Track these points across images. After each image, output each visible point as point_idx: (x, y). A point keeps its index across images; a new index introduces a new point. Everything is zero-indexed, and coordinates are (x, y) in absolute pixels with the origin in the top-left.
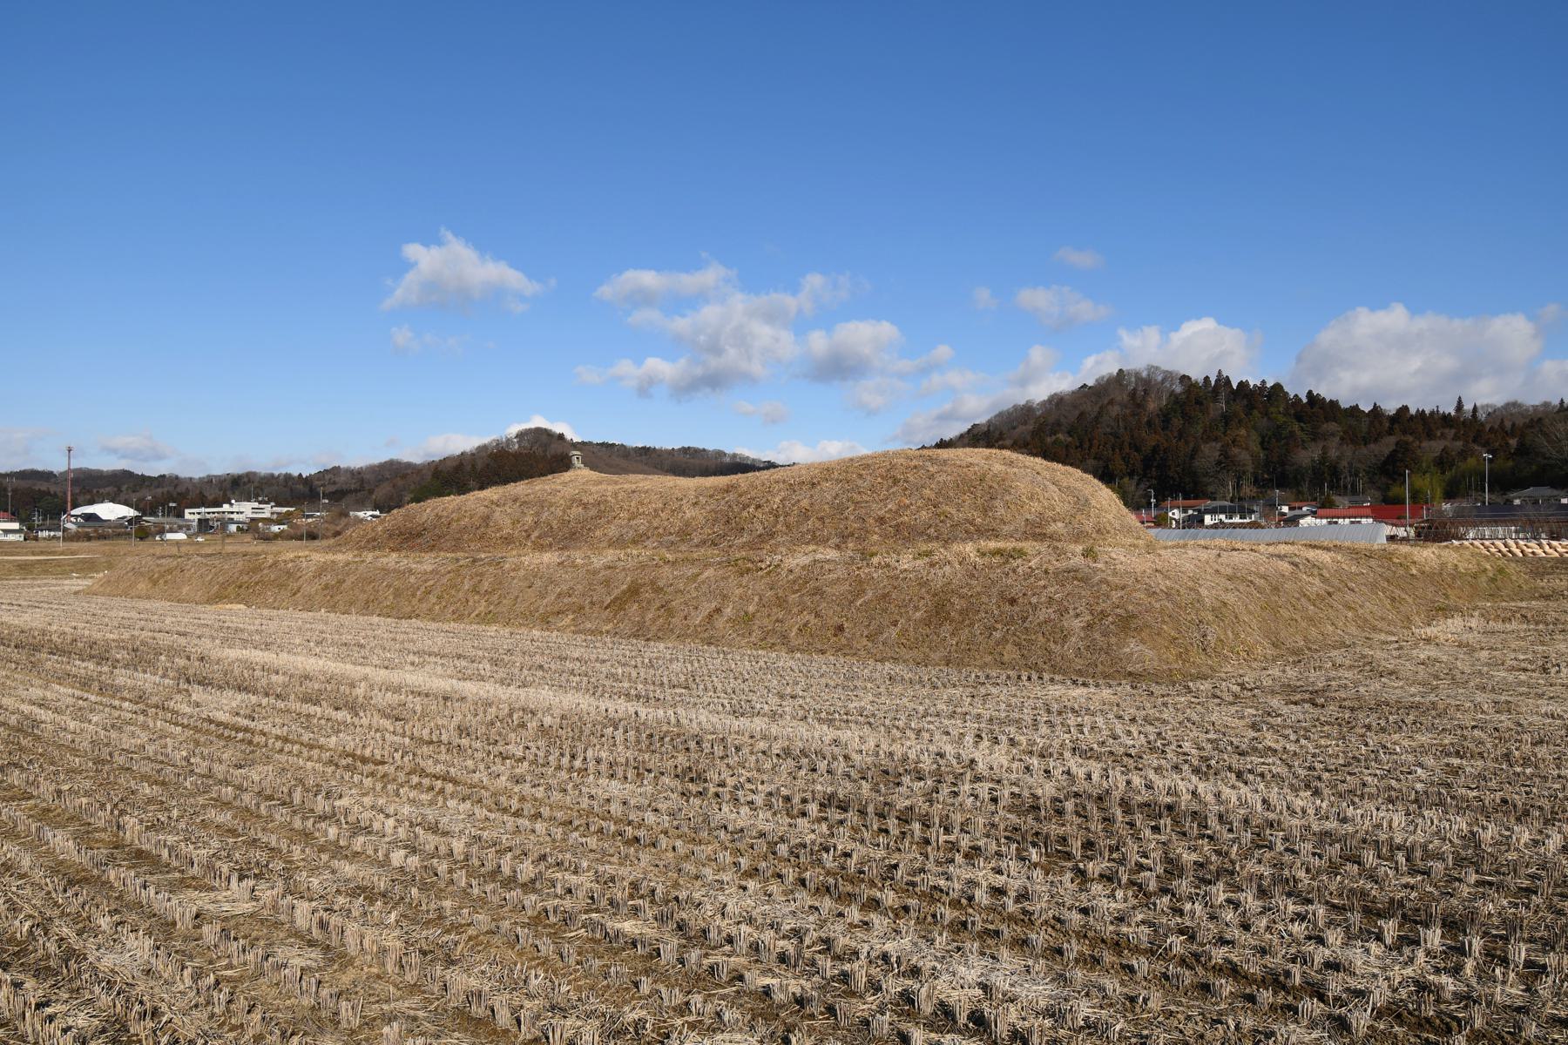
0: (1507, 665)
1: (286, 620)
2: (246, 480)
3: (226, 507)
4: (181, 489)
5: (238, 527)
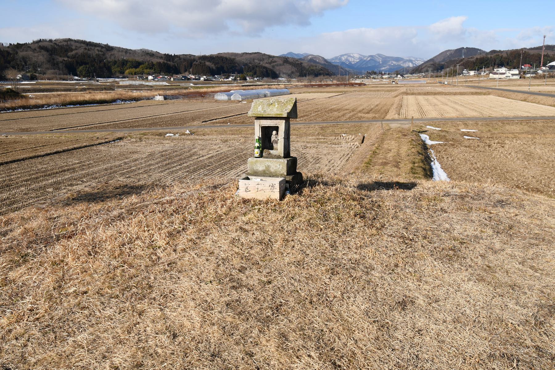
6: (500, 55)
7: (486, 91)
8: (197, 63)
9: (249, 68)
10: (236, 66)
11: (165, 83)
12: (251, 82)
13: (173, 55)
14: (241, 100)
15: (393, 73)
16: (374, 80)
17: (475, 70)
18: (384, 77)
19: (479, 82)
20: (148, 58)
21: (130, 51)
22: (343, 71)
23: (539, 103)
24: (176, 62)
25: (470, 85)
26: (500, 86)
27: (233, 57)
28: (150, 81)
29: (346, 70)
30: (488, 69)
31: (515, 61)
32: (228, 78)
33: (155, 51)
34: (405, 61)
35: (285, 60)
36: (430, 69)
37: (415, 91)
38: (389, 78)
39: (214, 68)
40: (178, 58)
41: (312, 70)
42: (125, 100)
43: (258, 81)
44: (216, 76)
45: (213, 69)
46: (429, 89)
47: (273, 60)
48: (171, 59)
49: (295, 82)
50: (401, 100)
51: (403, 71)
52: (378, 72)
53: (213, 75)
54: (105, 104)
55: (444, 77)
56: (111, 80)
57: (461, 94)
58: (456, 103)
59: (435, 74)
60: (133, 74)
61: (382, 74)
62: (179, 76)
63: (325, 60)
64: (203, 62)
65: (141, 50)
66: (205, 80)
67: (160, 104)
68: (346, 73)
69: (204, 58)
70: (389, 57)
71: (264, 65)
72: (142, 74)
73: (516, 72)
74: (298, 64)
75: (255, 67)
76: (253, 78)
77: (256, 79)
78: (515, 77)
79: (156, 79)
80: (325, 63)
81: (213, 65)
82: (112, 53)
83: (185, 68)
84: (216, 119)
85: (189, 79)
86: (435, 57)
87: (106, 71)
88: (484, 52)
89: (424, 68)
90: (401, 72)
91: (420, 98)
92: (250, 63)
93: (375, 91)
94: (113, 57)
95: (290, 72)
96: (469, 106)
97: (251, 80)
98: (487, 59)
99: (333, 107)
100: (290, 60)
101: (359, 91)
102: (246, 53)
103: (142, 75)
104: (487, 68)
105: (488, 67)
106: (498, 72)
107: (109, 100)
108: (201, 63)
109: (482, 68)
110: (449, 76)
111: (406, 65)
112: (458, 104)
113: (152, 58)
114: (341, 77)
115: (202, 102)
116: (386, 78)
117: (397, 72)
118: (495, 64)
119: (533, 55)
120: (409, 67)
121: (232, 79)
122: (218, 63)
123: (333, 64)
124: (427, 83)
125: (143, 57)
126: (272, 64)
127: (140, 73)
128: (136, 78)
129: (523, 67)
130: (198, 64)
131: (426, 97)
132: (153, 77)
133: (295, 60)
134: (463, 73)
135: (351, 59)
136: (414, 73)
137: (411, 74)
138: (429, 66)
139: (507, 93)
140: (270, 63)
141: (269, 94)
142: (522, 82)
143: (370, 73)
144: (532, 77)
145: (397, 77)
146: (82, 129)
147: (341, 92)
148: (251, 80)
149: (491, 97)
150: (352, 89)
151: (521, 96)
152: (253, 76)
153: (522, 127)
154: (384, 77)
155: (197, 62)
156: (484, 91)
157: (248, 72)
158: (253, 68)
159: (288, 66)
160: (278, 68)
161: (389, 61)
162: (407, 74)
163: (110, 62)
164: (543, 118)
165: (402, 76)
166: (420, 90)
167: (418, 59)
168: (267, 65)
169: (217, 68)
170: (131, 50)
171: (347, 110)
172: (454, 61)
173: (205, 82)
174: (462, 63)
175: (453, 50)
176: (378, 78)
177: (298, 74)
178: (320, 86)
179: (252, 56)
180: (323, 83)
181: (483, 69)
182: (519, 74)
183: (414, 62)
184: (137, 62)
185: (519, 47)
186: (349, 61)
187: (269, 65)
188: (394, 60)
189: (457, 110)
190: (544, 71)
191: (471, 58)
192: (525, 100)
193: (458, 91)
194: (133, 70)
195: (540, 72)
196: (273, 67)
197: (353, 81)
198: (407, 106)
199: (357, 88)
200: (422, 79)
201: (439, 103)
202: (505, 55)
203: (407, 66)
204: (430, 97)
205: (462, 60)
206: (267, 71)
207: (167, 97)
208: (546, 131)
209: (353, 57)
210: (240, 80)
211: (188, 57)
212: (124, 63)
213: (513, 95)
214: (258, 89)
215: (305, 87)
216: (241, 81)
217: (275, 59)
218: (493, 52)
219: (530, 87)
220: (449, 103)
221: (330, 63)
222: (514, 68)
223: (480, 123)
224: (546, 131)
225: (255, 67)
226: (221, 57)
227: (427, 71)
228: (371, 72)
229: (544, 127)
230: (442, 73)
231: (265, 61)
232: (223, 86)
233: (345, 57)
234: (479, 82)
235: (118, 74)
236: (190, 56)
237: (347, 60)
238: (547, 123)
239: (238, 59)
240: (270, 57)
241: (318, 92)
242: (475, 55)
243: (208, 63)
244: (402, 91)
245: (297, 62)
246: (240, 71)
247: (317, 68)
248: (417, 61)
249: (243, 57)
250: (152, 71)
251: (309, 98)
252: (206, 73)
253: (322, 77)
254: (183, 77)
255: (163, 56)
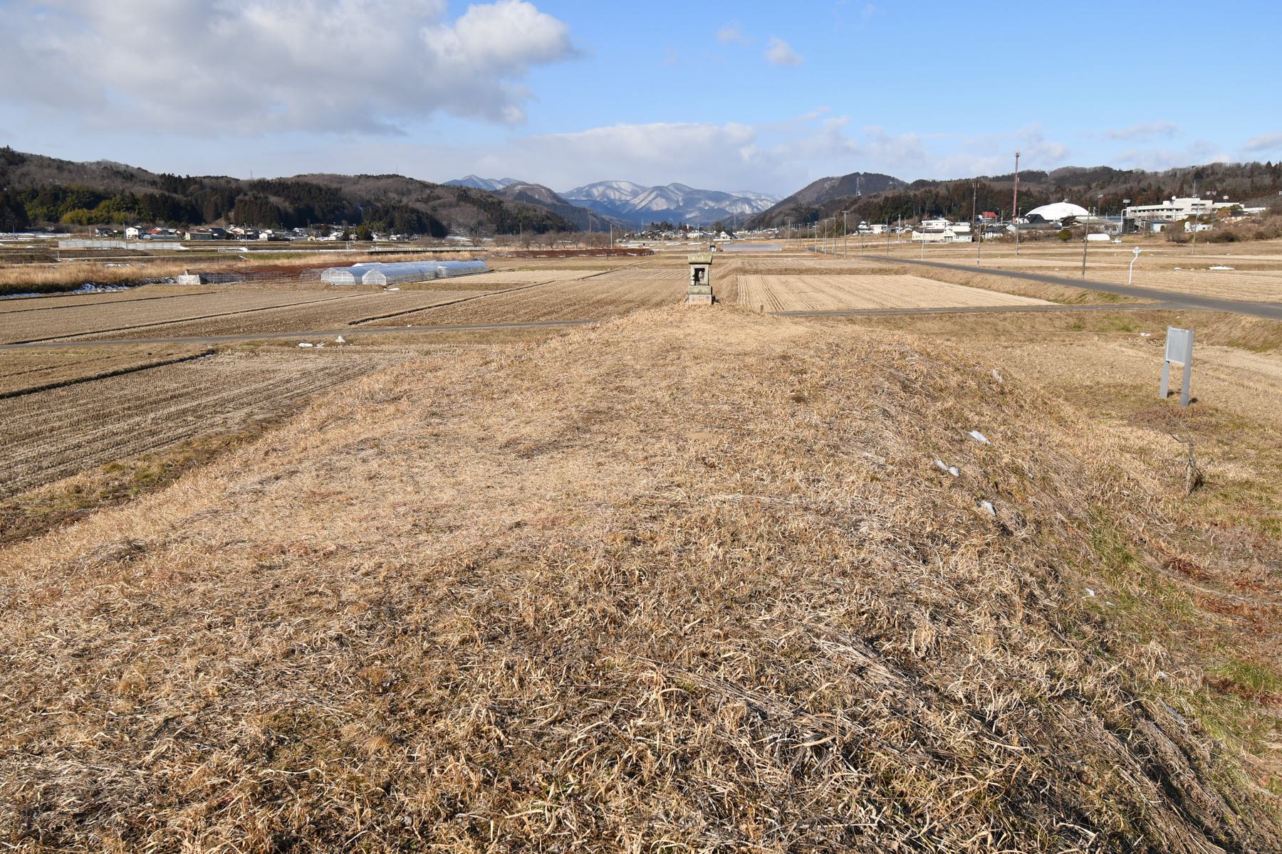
0: (365, 664)
1: (974, 303)
2: (1210, 171)
3: (1166, 204)
4: (1144, 184)
5: (1162, 227)
6: (934, 192)
7: (900, 266)
8: (247, 198)
9: (376, 210)
10: (344, 207)
11: (178, 246)
12: (384, 246)
13: (184, 177)
14: (384, 284)
15: (709, 227)
16: (669, 244)
17: (884, 222)
18: (689, 235)
19: (889, 248)
20: (118, 184)
21: (71, 167)
22: (597, 222)
23: (989, 288)
24: (191, 194)
25: (871, 254)
26: (931, 257)
27: (334, 186)
28: (132, 240)
29: (603, 219)
30: (910, 221)
31: (964, 204)
32: (327, 235)
33: (136, 166)
34: (736, 201)
35: (463, 194)
36: (789, 220)
37: (761, 267)
38: (702, 238)
39: (290, 210)
40: (197, 186)
41: (526, 218)
42: (104, 285)
43: (399, 241)
44: (297, 230)
45: (287, 213)
46: (789, 262)
47: (434, 194)
48: (180, 188)
49: (490, 245)
50: (736, 282)
51: (732, 223)
52: (676, 224)
53: (290, 229)
54: (57, 294)
55: (820, 236)
56: (25, 237)
57: (852, 272)
58: (839, 288)
59: (801, 231)
60: (85, 222)
61: (685, 229)
62: (207, 229)
63: (555, 196)
64: (261, 195)
65: (98, 163)
66: (270, 239)
67: (189, 292)
68: (605, 227)
69: (262, 186)
70: (699, 192)
71: (411, 205)
72: (108, 223)
73: (965, 227)
74: (493, 203)
75: (391, 209)
76: (388, 236)
77: (394, 237)
78: (963, 239)
79: (147, 237)
80: (555, 202)
81: (287, 204)
82: (25, 169)
83: (216, 210)
84: (373, 319)
85: (230, 236)
86: (799, 193)
87: (12, 215)
88: (902, 184)
89: (776, 216)
90: (728, 226)
91: (772, 279)
92: (377, 200)
93: (675, 266)
94: (27, 182)
95: (473, 222)
96: (863, 294)
97: (383, 240)
98: (908, 200)
99: (599, 297)
100: (473, 194)
101: (641, 267)
102: (367, 177)
103: (108, 226)
104: (908, 218)
105: (910, 217)
106: (930, 228)
107: (66, 284)
108: (256, 198)
109: (896, 219)
110: (830, 236)
111: (737, 210)
112: (844, 290)
113: (128, 185)
114: (594, 234)
115: (295, 288)
116: (695, 239)
117: (718, 224)
118: (923, 211)
119: (1000, 192)
120: (743, 213)
121: (337, 238)
122: (299, 198)
123: (573, 205)
124: (784, 251)
125: (105, 182)
126: (431, 204)
127: (102, 222)
128: (93, 232)
129: (980, 217)
130: (251, 202)
131: (783, 278)
132: (139, 229)
133: (484, 195)
134: (858, 229)
135: (613, 195)
136: (754, 228)
137: (749, 229)
138: (787, 212)
139: (938, 270)
140: (426, 201)
141: (444, 273)
142: (973, 249)
143: (658, 227)
144: (996, 239)
145: (718, 235)
146: (87, 339)
147: (602, 268)
148: (383, 240)
149: (908, 277)
150: (626, 262)
151: (961, 275)
152: (386, 231)
153: (942, 323)
154: (690, 235)
155: (245, 194)
156: (895, 266)
157: (373, 220)
158: (387, 212)
159: (470, 209)
160: (445, 212)
161: (700, 200)
162: (739, 229)
163: (19, 193)
164: (980, 310)
165: (730, 233)
166: (770, 263)
167: (763, 197)
168: (420, 206)
169: (298, 210)
170: (72, 163)
171: (631, 302)
172: (840, 201)
173: (272, 243)
174: (855, 206)
175: (837, 178)
176: (676, 239)
177: (494, 227)
178: (552, 254)
179: (381, 183)
180: (555, 248)
181: (899, 221)
182: (971, 232)
183: (754, 204)
184: (92, 193)
185: (973, 175)
186: (609, 198)
187: (424, 205)
188: (710, 199)
189: (840, 301)
190: (1020, 227)
191: (875, 196)
192: (967, 284)
193: (846, 267)
194: (83, 213)
195: (1011, 228)
196: (434, 209)
197: (623, 245)
198: (748, 294)
199: (635, 260)
200: (773, 242)
201: (808, 289)
202: (943, 192)
203: (739, 211)
204: (792, 279)
205: (855, 201)
206: (419, 219)
207: (209, 278)
208: (979, 330)
209: (618, 190)
210: (358, 239)
211: (223, 182)
212: (57, 197)
213: (948, 274)
214: (412, 260)
215: (518, 256)
216: (361, 242)
217: (437, 192)
218: (920, 183)
219: (981, 260)
220: (827, 289)
221: (565, 202)
222: (963, 220)
223: (875, 318)
224: (979, 330)
225: (391, 209)
226: (306, 184)
227: (784, 224)
228: (659, 223)
229: (976, 323)
230: (816, 227)
231: (414, 196)
232: (325, 254)
233: (601, 189)
234: (889, 248)
235: (42, 223)
236: (228, 180)
237: (604, 195)
238: (982, 317)
239: (347, 189)
240: (424, 185)
241: (552, 268)
242: (884, 190)
243: (273, 199)
244: (734, 266)
245: (490, 200)
246: (355, 219)
247: (538, 213)
248: (762, 200)
249: (359, 186)
250: (133, 215)
251: (539, 280)
252: (271, 221)
253: (551, 234)
254: (215, 230)
255: (158, 180)
